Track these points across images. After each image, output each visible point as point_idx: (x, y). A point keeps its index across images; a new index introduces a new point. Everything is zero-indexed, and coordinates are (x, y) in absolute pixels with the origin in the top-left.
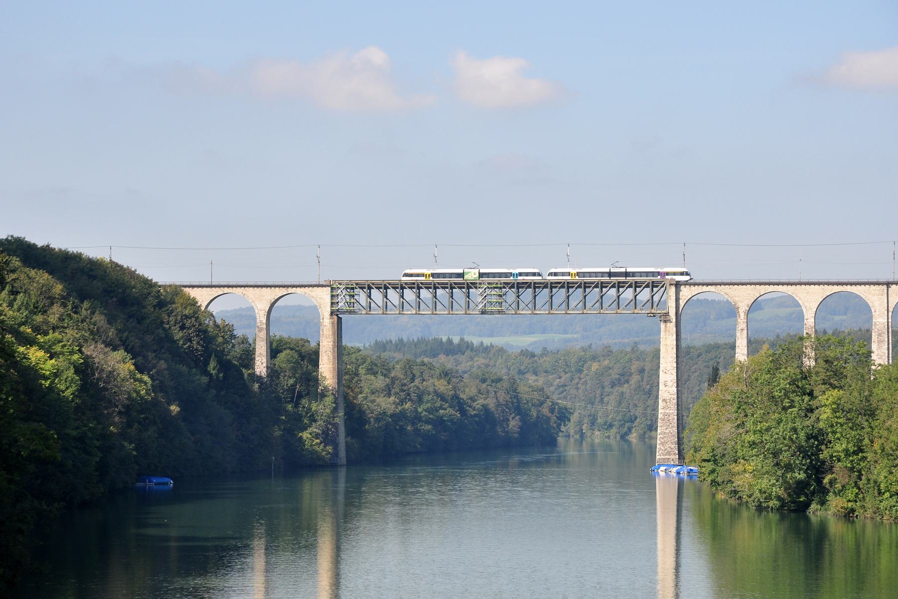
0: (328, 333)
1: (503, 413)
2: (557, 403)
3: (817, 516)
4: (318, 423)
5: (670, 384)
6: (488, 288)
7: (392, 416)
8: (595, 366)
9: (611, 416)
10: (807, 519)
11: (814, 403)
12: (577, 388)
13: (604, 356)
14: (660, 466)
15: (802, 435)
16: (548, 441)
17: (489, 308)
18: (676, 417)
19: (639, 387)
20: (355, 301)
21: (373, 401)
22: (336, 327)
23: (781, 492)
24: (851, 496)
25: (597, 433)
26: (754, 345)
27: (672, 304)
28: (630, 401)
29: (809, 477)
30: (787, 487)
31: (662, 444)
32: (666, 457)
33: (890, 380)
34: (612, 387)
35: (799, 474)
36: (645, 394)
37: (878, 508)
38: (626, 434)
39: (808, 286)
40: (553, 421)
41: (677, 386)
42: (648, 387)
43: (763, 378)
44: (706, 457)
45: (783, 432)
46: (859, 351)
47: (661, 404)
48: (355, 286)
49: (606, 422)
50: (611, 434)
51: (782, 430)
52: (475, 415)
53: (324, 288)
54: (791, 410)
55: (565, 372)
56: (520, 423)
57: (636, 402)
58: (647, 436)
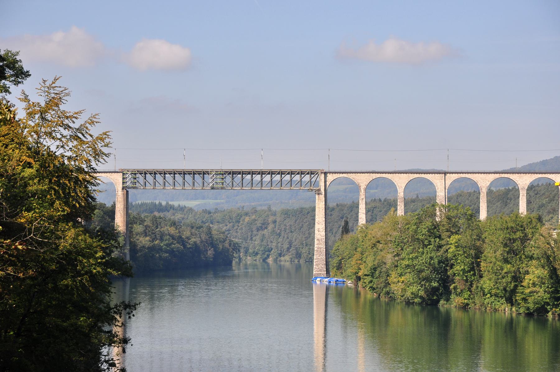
0: (121, 200)
1: (205, 246)
2: (232, 241)
3: (444, 308)
4: (115, 253)
5: (321, 230)
6: (216, 174)
7: (149, 248)
8: (247, 219)
9: (257, 248)
10: (438, 309)
11: (443, 242)
12: (237, 232)
13: (252, 213)
14: (316, 278)
15: (436, 261)
16: (228, 264)
17: (215, 186)
18: (325, 250)
19: (273, 231)
20: (136, 181)
21: (138, 240)
22: (125, 196)
23: (422, 293)
24: (466, 296)
25: (249, 258)
26: (340, 207)
28: (269, 240)
29: (440, 285)
30: (426, 291)
31: (317, 265)
32: (319, 273)
33: (496, 230)
34: (257, 231)
35: (435, 283)
36: (277, 235)
37: (483, 303)
38: (266, 258)
39: (400, 174)
40: (230, 251)
41: (326, 232)
42: (279, 231)
43: (412, 228)
44: (366, 273)
45: (425, 259)
46: (466, 212)
47: (316, 242)
48: (137, 172)
49: (254, 252)
50: (257, 259)
51: (425, 258)
52: (190, 248)
53: (118, 174)
54: (429, 246)
55: (229, 222)
56: (214, 253)
57: (272, 240)
58: (278, 260)
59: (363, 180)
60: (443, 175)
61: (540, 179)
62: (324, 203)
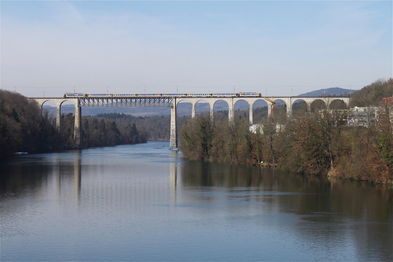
5: (174, 125)
27: (174, 103)
41: (176, 126)
47: (171, 131)
59: (251, 101)
60: (232, 98)
61: (335, 101)
62: (175, 112)
